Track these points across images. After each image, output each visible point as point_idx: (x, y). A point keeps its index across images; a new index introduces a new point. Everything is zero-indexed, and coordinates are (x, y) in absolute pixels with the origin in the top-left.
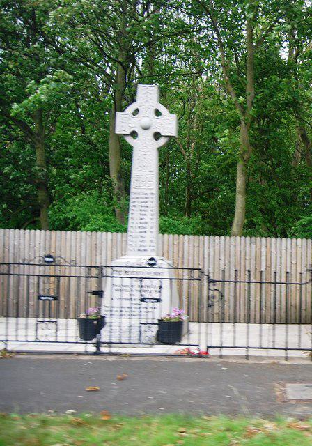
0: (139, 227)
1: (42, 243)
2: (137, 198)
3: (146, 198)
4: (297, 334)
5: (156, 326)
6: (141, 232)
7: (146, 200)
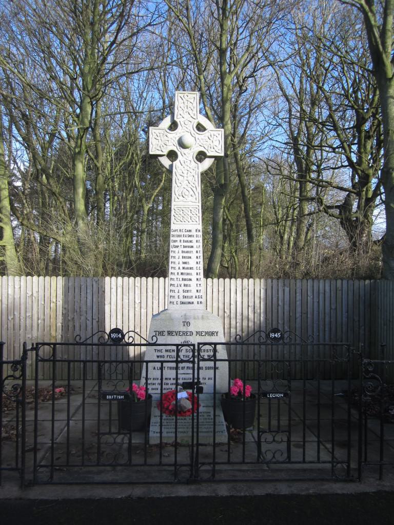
0: (182, 274)
1: (41, 293)
2: (179, 236)
3: (190, 236)
4: (302, 435)
5: (159, 442)
6: (185, 280)
7: (190, 239)
